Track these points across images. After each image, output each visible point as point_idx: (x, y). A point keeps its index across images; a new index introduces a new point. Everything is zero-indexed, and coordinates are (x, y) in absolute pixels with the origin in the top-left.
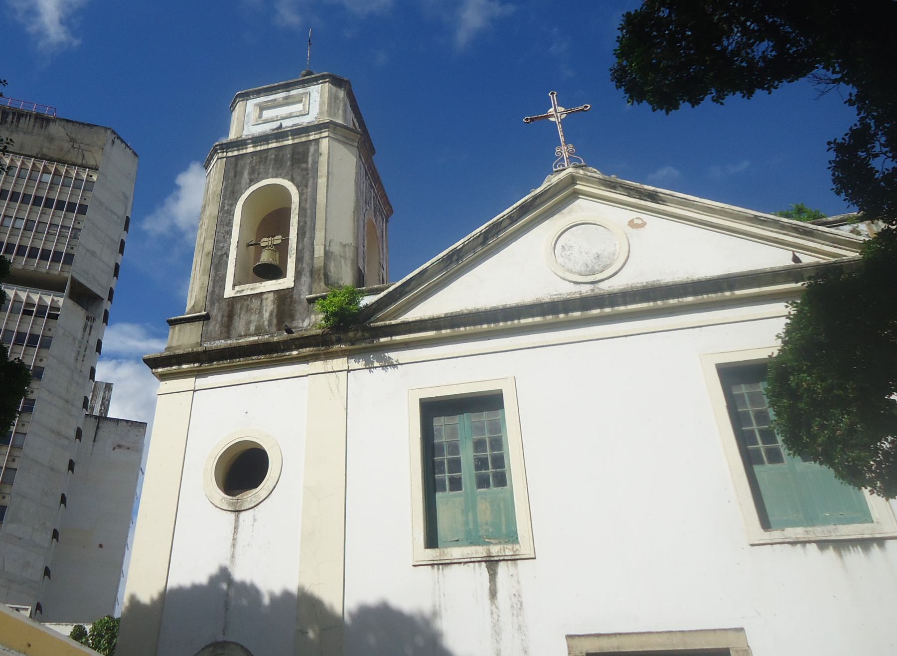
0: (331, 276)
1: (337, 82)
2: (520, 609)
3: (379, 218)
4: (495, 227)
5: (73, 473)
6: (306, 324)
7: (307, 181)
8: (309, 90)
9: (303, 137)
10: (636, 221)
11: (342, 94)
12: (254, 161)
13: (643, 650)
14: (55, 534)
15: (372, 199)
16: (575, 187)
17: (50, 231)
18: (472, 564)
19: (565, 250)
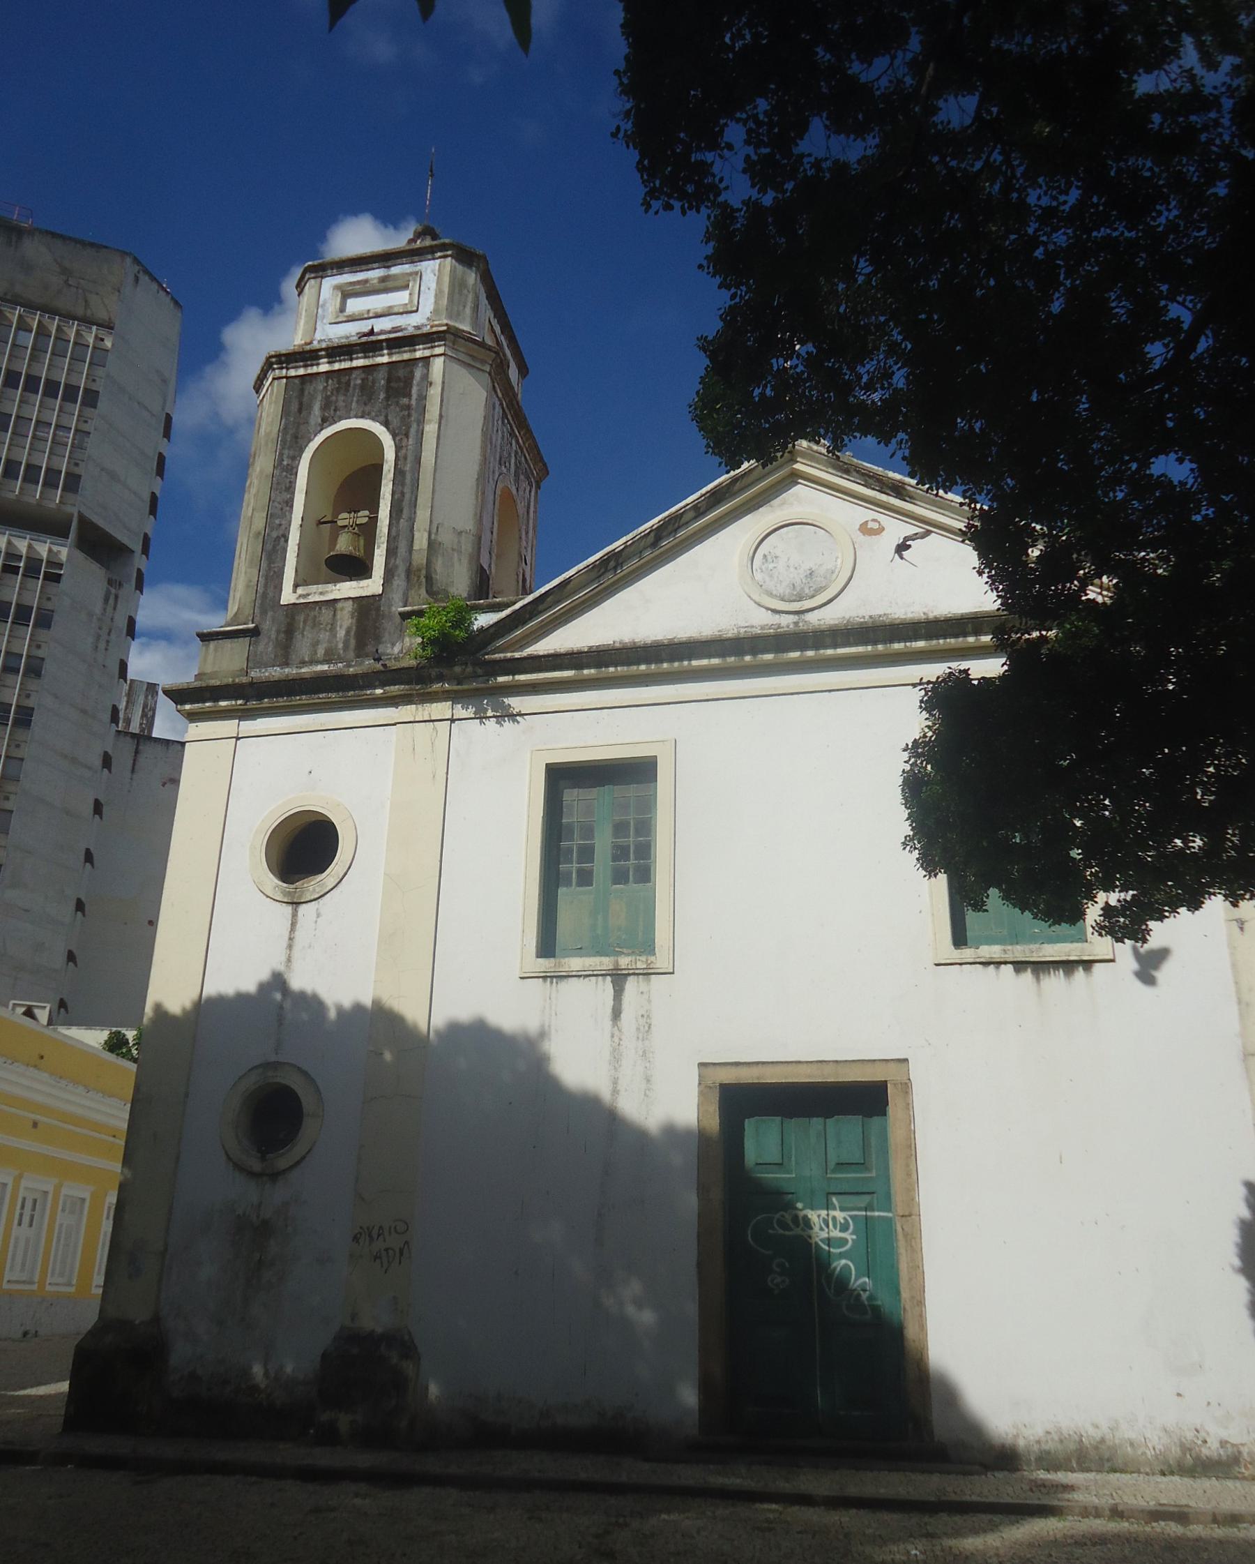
0: (437, 580)
1: (465, 256)
2: (647, 1032)
3: (524, 484)
4: (673, 522)
5: (101, 818)
6: (396, 649)
7: (409, 427)
8: (419, 268)
9: (405, 352)
10: (871, 525)
11: (472, 277)
12: (329, 388)
13: (787, 1081)
14: (80, 906)
15: (513, 455)
16: (794, 466)
17: (38, 433)
18: (594, 978)
19: (767, 560)
